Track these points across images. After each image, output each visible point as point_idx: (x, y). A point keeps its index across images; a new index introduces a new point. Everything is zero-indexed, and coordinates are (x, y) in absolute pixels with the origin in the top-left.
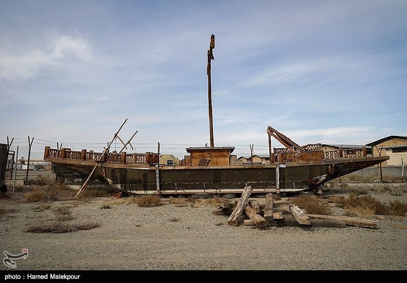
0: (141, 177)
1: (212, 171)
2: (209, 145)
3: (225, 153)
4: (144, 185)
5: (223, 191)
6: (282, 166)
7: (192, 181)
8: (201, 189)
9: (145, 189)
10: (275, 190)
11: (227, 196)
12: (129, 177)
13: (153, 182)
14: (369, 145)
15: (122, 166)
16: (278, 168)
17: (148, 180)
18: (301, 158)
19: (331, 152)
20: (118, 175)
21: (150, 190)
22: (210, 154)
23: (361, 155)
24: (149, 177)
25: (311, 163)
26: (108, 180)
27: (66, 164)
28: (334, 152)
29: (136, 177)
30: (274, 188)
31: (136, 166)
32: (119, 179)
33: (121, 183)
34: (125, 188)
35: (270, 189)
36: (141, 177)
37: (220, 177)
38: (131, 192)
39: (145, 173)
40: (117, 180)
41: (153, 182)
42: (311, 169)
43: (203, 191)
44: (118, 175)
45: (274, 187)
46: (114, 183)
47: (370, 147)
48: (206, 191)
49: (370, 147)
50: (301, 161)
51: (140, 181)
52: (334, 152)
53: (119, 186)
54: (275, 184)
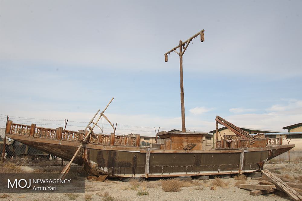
0: (131, 160)
1: (137, 154)
2: (180, 128)
3: (199, 138)
4: (133, 168)
5: (202, 173)
6: (246, 151)
7: (177, 164)
8: (184, 171)
9: (134, 173)
10: (238, 171)
11: (204, 178)
12: (118, 160)
13: (142, 165)
14: (211, 132)
15: (112, 148)
16: (243, 153)
17: (138, 163)
18: (254, 144)
19: (272, 139)
20: (106, 157)
21: (139, 173)
22: (187, 138)
23: (270, 143)
24: (139, 160)
25: (262, 149)
26: (92, 162)
27: (36, 143)
28: (26, 127)
29: (126, 160)
30: (238, 170)
31: (126, 149)
32: (106, 162)
33: (109, 166)
34: (113, 172)
35: (235, 170)
36: (131, 160)
37: (200, 161)
38: (119, 175)
39: (135, 156)
40: (104, 162)
41: (142, 165)
42: (261, 154)
43: (185, 173)
44: (106, 157)
45: (238, 169)
46: (100, 166)
47: (212, 134)
48: (189, 173)
49: (212, 134)
50: (254, 147)
51: (129, 165)
52: (26, 127)
53: (105, 170)
54: (239, 167)
